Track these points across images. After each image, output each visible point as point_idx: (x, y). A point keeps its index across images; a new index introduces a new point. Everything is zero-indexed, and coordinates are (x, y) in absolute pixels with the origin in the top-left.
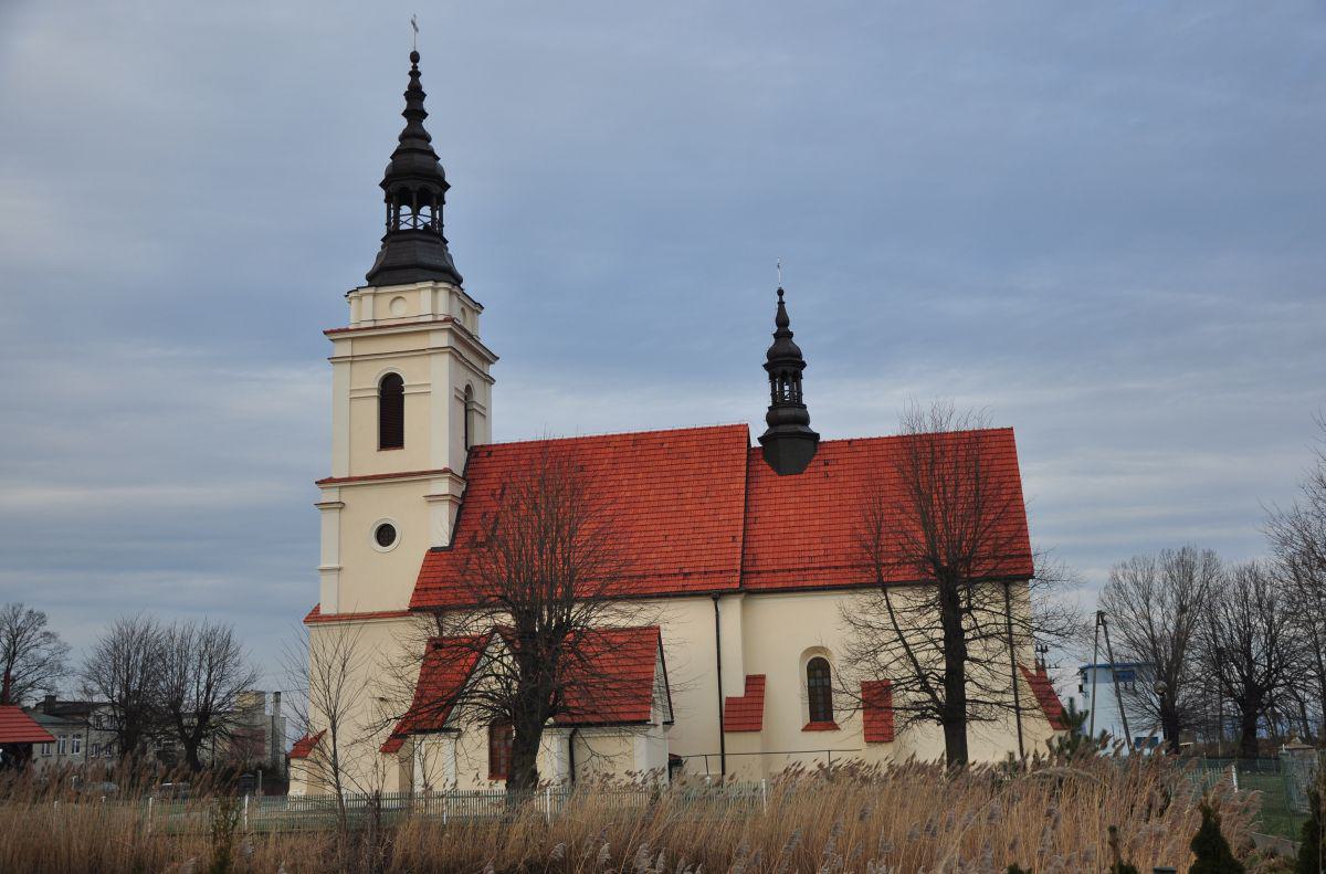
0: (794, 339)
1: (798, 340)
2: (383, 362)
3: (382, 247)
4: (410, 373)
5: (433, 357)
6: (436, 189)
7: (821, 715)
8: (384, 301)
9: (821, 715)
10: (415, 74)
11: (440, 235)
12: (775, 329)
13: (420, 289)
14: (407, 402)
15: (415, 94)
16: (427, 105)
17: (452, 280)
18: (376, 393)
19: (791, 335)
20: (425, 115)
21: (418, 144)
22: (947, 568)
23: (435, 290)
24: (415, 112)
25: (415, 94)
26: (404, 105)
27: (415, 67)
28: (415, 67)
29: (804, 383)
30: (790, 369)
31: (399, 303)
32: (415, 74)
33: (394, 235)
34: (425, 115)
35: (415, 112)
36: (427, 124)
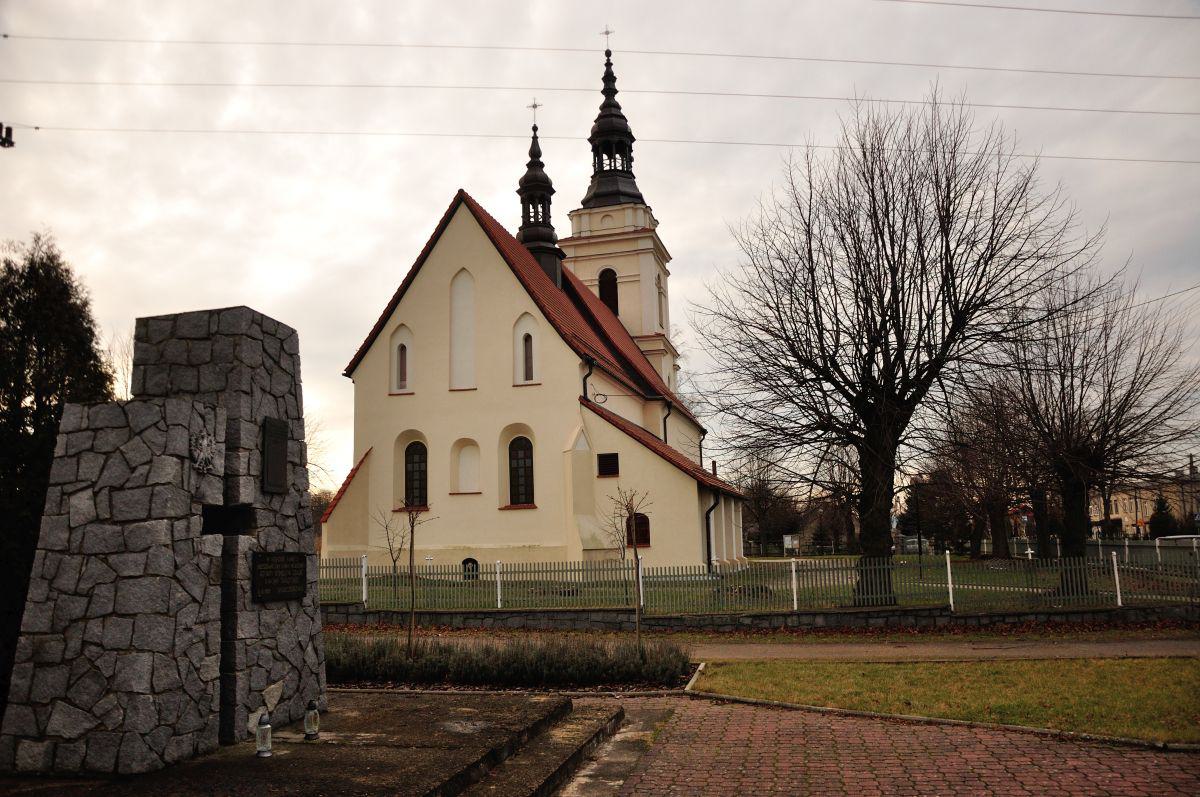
0: (545, 170)
1: (548, 170)
2: (604, 260)
3: (592, 182)
4: (622, 268)
5: (641, 256)
6: (624, 139)
7: (523, 498)
8: (597, 218)
9: (523, 498)
10: (609, 65)
11: (631, 173)
12: (529, 159)
13: (624, 209)
14: (619, 286)
15: (609, 78)
16: (617, 85)
17: (631, 200)
18: (597, 283)
19: (542, 165)
20: (616, 92)
21: (614, 111)
22: (977, 504)
23: (636, 209)
24: (610, 90)
25: (609, 78)
26: (602, 86)
27: (608, 60)
28: (608, 60)
29: (552, 208)
30: (539, 193)
31: (607, 219)
32: (609, 65)
33: (599, 174)
34: (616, 92)
35: (610, 90)
36: (617, 98)
